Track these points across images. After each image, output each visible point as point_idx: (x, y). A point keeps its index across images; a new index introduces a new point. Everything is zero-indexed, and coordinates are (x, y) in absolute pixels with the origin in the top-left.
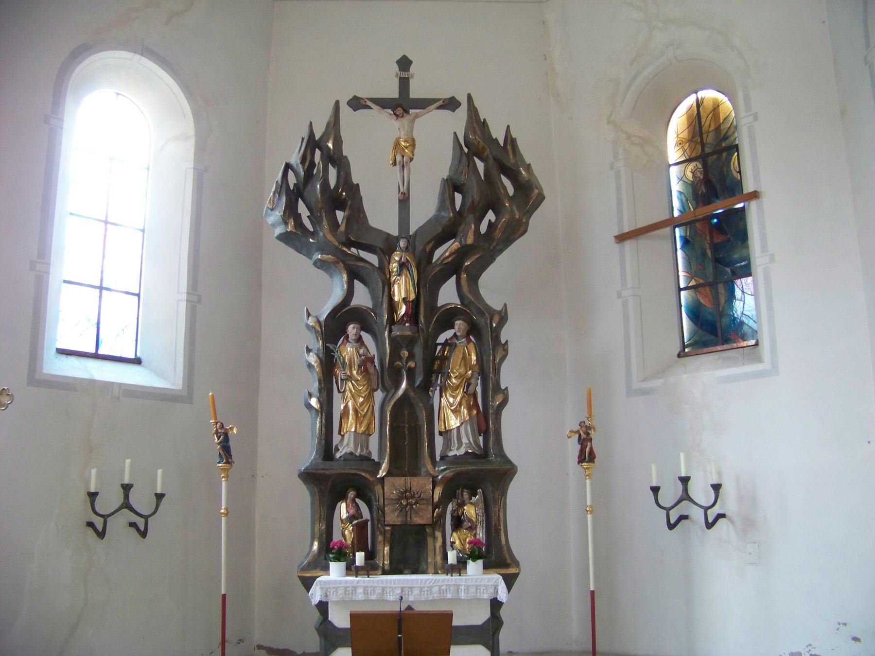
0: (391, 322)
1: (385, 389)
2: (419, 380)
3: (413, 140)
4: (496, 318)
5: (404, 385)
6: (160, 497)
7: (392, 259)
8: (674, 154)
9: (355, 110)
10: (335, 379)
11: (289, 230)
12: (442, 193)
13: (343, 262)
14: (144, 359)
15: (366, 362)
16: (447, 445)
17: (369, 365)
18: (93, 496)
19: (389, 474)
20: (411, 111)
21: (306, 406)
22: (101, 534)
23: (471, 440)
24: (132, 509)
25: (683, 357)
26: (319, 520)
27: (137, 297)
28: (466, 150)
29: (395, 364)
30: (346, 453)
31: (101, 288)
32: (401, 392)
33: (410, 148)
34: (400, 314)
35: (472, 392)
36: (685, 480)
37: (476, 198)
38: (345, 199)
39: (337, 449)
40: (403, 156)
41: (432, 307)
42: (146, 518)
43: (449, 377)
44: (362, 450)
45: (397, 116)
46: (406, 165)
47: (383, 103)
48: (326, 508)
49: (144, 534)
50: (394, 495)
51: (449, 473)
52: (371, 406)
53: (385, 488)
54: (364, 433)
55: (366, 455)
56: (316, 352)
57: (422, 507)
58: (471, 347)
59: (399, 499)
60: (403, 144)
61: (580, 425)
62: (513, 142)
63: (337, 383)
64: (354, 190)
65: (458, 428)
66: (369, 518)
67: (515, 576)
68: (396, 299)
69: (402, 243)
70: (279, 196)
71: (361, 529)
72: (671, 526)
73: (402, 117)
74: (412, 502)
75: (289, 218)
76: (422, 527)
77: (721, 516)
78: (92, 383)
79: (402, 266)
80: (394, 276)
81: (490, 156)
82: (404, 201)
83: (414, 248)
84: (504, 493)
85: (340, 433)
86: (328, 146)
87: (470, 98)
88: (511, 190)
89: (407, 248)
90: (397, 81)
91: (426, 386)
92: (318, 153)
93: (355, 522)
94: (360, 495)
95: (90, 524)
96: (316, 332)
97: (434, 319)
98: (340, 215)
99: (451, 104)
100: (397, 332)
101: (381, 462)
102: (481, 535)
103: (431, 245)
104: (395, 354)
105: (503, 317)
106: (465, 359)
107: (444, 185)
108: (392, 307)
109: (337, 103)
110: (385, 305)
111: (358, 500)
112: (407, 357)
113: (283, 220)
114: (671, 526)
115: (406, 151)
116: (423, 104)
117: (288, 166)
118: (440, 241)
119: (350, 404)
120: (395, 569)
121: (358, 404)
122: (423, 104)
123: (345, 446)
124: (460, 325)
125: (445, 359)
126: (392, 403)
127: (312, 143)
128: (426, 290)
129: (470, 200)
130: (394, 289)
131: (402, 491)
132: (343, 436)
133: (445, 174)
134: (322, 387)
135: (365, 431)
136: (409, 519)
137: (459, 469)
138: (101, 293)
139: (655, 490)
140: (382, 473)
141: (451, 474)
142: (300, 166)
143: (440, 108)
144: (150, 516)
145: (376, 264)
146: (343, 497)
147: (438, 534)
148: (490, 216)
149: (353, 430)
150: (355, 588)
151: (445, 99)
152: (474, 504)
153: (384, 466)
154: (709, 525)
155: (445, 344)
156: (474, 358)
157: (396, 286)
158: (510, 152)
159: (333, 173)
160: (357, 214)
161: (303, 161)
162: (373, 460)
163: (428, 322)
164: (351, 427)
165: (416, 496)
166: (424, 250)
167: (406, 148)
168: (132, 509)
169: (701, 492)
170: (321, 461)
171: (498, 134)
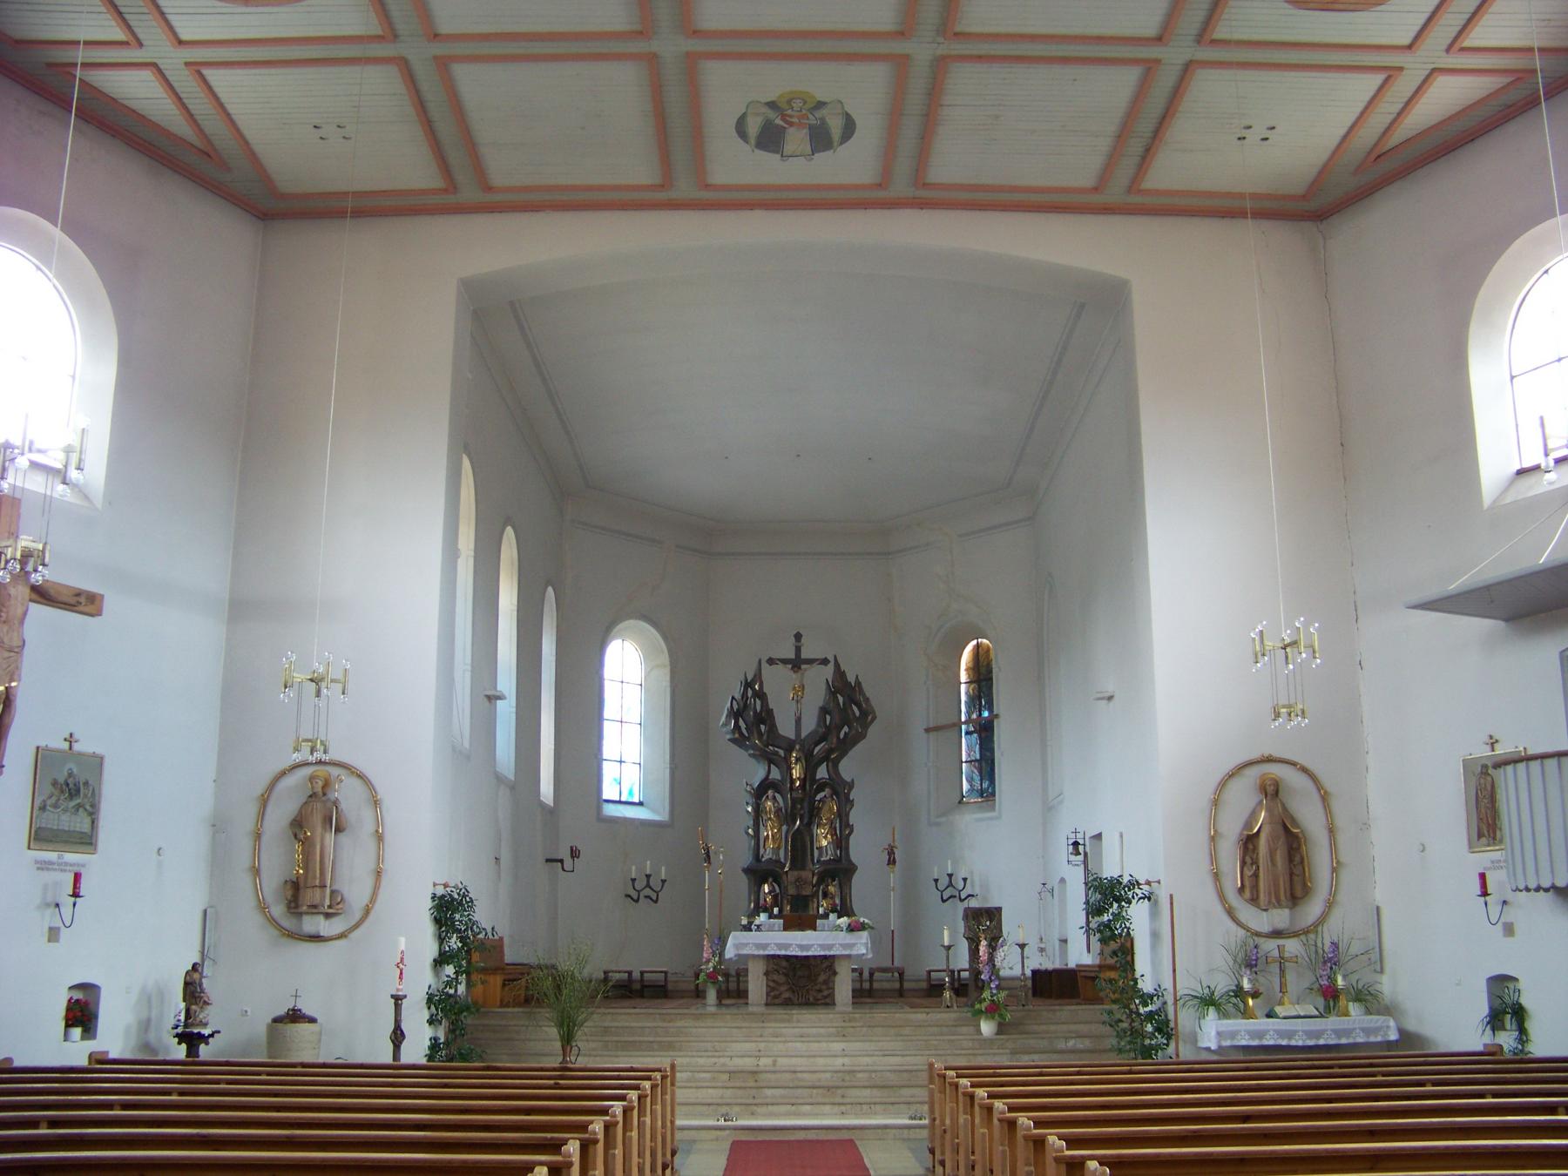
0: (792, 789)
1: (788, 825)
2: (806, 821)
4: (847, 787)
5: (798, 823)
6: (664, 881)
8: (964, 677)
14: (645, 802)
15: (778, 811)
16: (820, 855)
18: (633, 880)
20: (803, 667)
24: (650, 888)
25: (93, 823)
32: (796, 827)
36: (648, 876)
39: (762, 856)
41: (814, 780)
43: (822, 819)
47: (785, 661)
51: (821, 869)
58: (834, 803)
64: (770, 713)
65: (826, 846)
69: (797, 747)
71: (775, 898)
72: (944, 901)
76: (807, 896)
77: (969, 896)
78: (625, 820)
79: (798, 760)
82: (798, 721)
84: (850, 880)
88: (857, 713)
91: (809, 824)
92: (749, 690)
94: (775, 881)
99: (825, 662)
100: (794, 794)
102: (838, 901)
105: (851, 785)
106: (831, 809)
108: (792, 781)
109: (760, 661)
114: (944, 901)
116: (810, 662)
118: (817, 744)
119: (770, 833)
123: (767, 854)
125: (820, 809)
127: (748, 685)
133: (821, 704)
140: (786, 869)
145: (783, 755)
146: (765, 881)
147: (815, 900)
148: (846, 729)
150: (774, 925)
152: (834, 886)
155: (819, 801)
157: (794, 771)
160: (772, 727)
163: (811, 786)
166: (809, 750)
168: (650, 888)
171: (851, 679)
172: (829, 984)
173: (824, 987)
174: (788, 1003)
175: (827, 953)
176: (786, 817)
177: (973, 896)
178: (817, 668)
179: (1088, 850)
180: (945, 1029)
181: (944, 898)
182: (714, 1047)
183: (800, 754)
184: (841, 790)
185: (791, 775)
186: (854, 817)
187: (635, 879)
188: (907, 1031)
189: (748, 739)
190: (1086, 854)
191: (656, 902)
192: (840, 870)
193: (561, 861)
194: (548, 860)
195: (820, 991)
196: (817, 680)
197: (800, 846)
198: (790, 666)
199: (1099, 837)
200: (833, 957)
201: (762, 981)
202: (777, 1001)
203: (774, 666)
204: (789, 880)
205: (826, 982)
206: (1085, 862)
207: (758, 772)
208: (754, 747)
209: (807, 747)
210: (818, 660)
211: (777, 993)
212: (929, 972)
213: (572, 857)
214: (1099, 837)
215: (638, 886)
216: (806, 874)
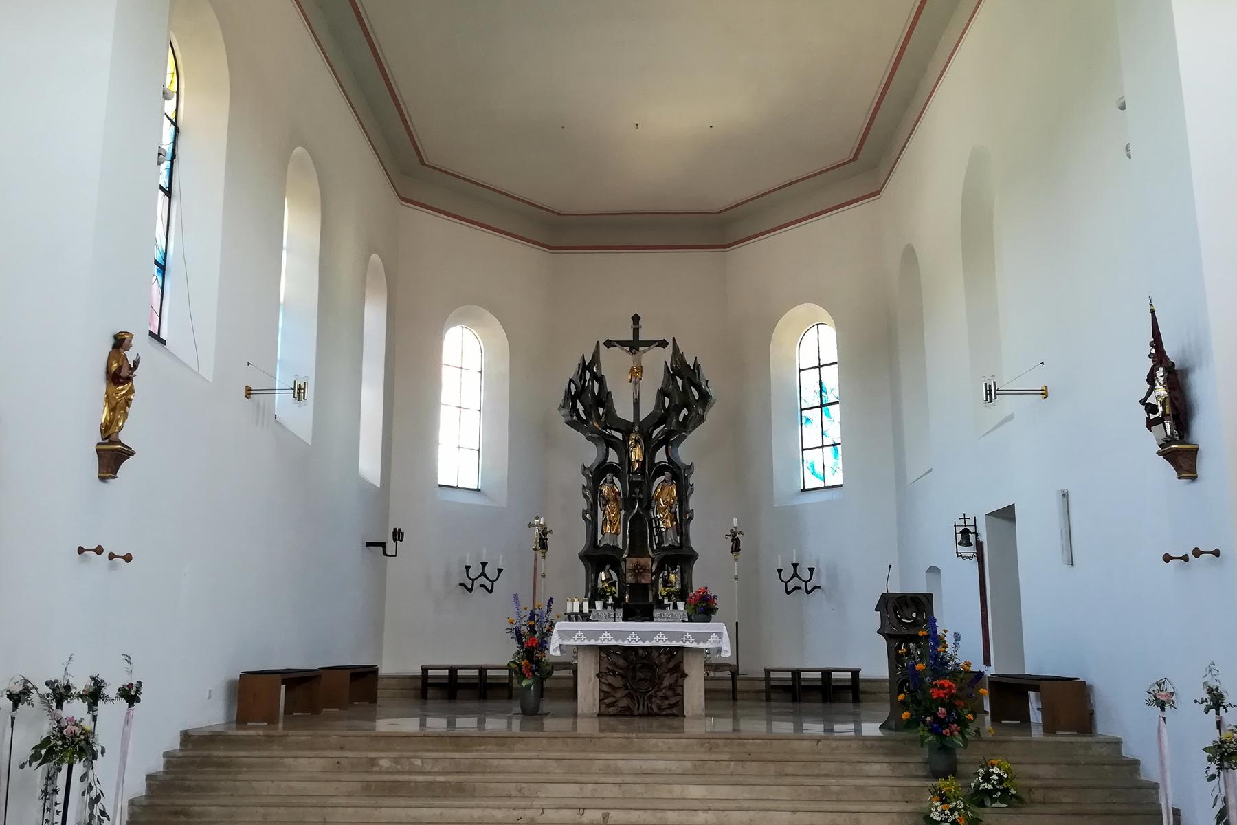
12: (658, 399)
13: (604, 438)
17: (618, 496)
20: (641, 349)
32: (635, 512)
47: (623, 344)
50: (518, 686)
54: (615, 533)
68: (633, 460)
69: (636, 429)
72: (788, 593)
76: (646, 585)
79: (637, 442)
82: (636, 404)
88: (697, 397)
89: (638, 432)
98: (601, 410)
99: (663, 344)
104: (632, 491)
106: (670, 493)
108: (631, 464)
114: (788, 593)
116: (648, 344)
117: (571, 380)
119: (608, 517)
127: (584, 367)
139: (780, 571)
140: (625, 556)
143: (657, 346)
146: (603, 569)
148: (685, 411)
152: (676, 574)
153: (626, 551)
156: (675, 492)
159: (596, 385)
160: (610, 411)
171: (690, 362)
172: (676, 690)
173: (670, 693)
174: (626, 713)
175: (674, 644)
176: (628, 503)
177: (819, 587)
178: (655, 351)
179: (983, 538)
180: (847, 767)
181: (789, 590)
182: (520, 791)
183: (638, 437)
184: (679, 475)
185: (630, 459)
186: (693, 503)
187: (470, 567)
188: (790, 768)
189: (586, 422)
190: (979, 545)
191: (490, 591)
192: (682, 557)
193: (383, 545)
194: (368, 544)
195: (666, 698)
196: (655, 362)
197: (639, 529)
198: (628, 348)
199: (1007, 514)
200: (681, 648)
201: (595, 682)
202: (611, 710)
205: (671, 687)
206: (980, 555)
207: (590, 454)
208: (594, 431)
209: (645, 430)
211: (611, 699)
212: (768, 671)
213: (395, 540)
214: (1007, 514)
215: (473, 573)
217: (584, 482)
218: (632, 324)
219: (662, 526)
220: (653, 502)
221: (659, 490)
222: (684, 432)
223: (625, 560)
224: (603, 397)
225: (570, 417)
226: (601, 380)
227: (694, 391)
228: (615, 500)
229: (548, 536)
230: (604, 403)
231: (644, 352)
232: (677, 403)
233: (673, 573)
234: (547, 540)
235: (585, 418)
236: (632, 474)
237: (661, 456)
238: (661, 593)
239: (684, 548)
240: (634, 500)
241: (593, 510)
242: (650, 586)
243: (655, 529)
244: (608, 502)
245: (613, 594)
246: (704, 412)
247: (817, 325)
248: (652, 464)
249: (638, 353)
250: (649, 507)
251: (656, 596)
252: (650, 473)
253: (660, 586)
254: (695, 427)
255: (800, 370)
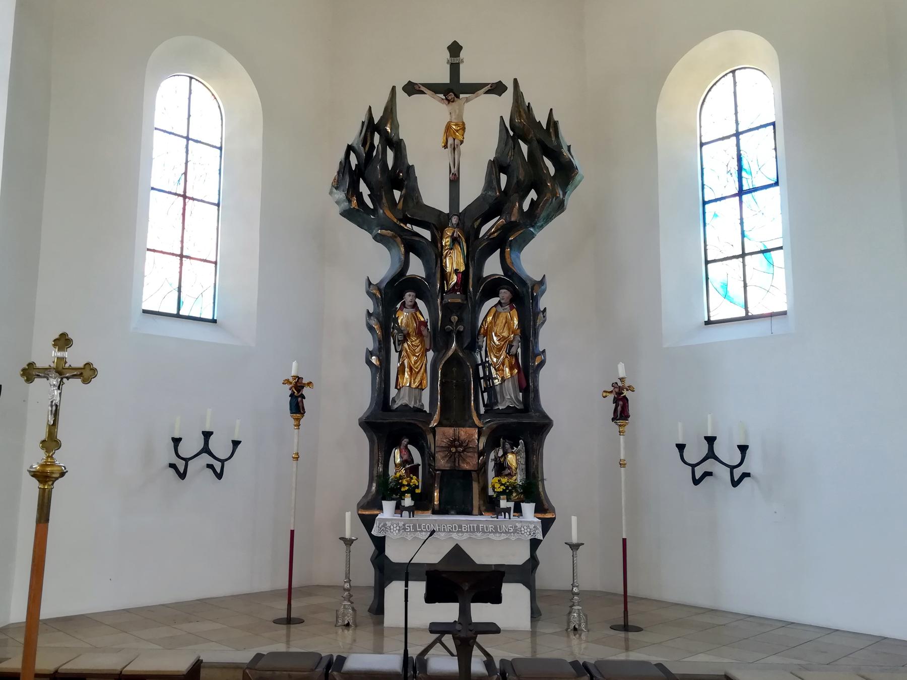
3: (464, 124)
7: (445, 234)
9: (409, 95)
10: (393, 339)
11: (513, 219)
13: (401, 237)
17: (423, 328)
19: (440, 424)
20: (461, 96)
21: (367, 363)
22: (182, 476)
23: (513, 396)
26: (377, 464)
27: (214, 265)
28: (511, 133)
29: (446, 328)
30: (401, 405)
31: (181, 256)
32: (450, 353)
33: (461, 131)
34: (451, 283)
35: (515, 352)
36: (711, 440)
37: (521, 177)
38: (402, 179)
39: (394, 401)
40: (454, 139)
42: (223, 462)
44: (415, 402)
45: (449, 101)
46: (457, 148)
47: (435, 88)
48: (383, 453)
49: (219, 476)
51: (493, 424)
52: (424, 365)
53: (436, 437)
54: (417, 388)
55: (419, 407)
56: (377, 316)
57: (469, 454)
58: (514, 312)
59: (448, 448)
60: (454, 127)
61: (612, 386)
62: (556, 124)
63: (394, 343)
64: (410, 169)
66: (420, 462)
67: (552, 520)
68: (449, 269)
69: (455, 220)
70: (343, 176)
72: (696, 482)
73: (453, 102)
74: (460, 450)
75: (352, 196)
76: (468, 473)
79: (455, 240)
80: (446, 250)
81: (535, 139)
82: (454, 182)
83: (463, 224)
85: (396, 387)
86: (386, 129)
87: (516, 82)
88: (552, 171)
89: (458, 225)
90: (448, 66)
92: (377, 137)
93: (408, 466)
95: (172, 466)
96: (377, 298)
97: (481, 288)
98: (397, 194)
99: (498, 89)
100: (449, 299)
101: (432, 413)
103: (479, 221)
104: (446, 319)
106: (508, 323)
107: (492, 167)
108: (444, 276)
109: (394, 88)
110: (438, 275)
111: (410, 447)
112: (457, 322)
113: (347, 197)
114: (696, 482)
115: (457, 134)
116: (473, 89)
117: (350, 148)
119: (406, 362)
120: (442, 510)
121: (413, 363)
122: (473, 89)
124: (505, 294)
126: (443, 362)
127: (371, 127)
128: (474, 262)
129: (515, 181)
130: (446, 261)
131: (452, 439)
132: (399, 390)
134: (381, 347)
135: (419, 385)
136: (457, 465)
137: (530, 287)
138: (181, 260)
139: (681, 447)
140: (433, 424)
141: (495, 426)
142: (362, 148)
143: (487, 92)
144: (227, 460)
146: (397, 444)
148: (533, 195)
149: (408, 385)
151: (493, 83)
152: (517, 454)
154: (735, 483)
156: (516, 322)
158: (553, 135)
159: (390, 155)
161: (364, 145)
162: (425, 411)
164: (406, 383)
165: (464, 445)
167: (457, 131)
169: (727, 451)
170: (381, 412)
171: (541, 117)
186: (545, 339)
203: (416, 97)
204: (438, 443)
209: (468, 224)
210: (486, 85)
215: (187, 450)
216: (467, 433)
217: (370, 305)
218: (449, 57)
219: (494, 375)
220: (481, 338)
221: (490, 319)
222: (533, 226)
223: (433, 430)
224: (400, 172)
225: (346, 204)
226: (398, 146)
227: (548, 163)
228: (419, 334)
229: (306, 391)
230: (402, 180)
231: (467, 100)
232: (521, 177)
233: (513, 453)
234: (304, 397)
235: (372, 207)
236: (450, 291)
237: (492, 266)
238: (494, 488)
239: (532, 413)
240: (448, 334)
241: (383, 350)
242: (474, 475)
243: (482, 381)
244: (406, 337)
245: (412, 491)
246: (564, 194)
247: (733, 72)
248: (479, 278)
249: (458, 102)
250: (473, 346)
251: (484, 489)
252: (475, 291)
253: (491, 473)
254: (549, 219)
255: (702, 145)
